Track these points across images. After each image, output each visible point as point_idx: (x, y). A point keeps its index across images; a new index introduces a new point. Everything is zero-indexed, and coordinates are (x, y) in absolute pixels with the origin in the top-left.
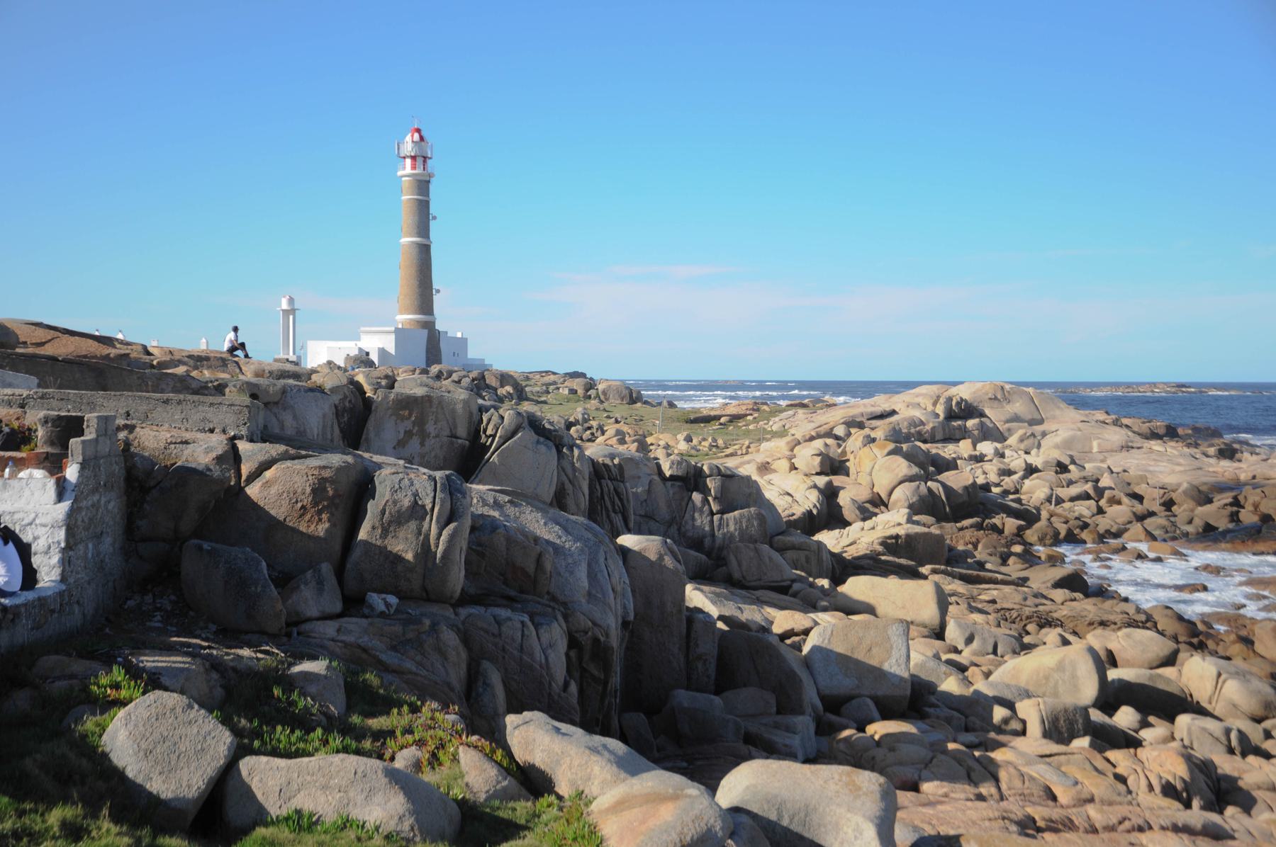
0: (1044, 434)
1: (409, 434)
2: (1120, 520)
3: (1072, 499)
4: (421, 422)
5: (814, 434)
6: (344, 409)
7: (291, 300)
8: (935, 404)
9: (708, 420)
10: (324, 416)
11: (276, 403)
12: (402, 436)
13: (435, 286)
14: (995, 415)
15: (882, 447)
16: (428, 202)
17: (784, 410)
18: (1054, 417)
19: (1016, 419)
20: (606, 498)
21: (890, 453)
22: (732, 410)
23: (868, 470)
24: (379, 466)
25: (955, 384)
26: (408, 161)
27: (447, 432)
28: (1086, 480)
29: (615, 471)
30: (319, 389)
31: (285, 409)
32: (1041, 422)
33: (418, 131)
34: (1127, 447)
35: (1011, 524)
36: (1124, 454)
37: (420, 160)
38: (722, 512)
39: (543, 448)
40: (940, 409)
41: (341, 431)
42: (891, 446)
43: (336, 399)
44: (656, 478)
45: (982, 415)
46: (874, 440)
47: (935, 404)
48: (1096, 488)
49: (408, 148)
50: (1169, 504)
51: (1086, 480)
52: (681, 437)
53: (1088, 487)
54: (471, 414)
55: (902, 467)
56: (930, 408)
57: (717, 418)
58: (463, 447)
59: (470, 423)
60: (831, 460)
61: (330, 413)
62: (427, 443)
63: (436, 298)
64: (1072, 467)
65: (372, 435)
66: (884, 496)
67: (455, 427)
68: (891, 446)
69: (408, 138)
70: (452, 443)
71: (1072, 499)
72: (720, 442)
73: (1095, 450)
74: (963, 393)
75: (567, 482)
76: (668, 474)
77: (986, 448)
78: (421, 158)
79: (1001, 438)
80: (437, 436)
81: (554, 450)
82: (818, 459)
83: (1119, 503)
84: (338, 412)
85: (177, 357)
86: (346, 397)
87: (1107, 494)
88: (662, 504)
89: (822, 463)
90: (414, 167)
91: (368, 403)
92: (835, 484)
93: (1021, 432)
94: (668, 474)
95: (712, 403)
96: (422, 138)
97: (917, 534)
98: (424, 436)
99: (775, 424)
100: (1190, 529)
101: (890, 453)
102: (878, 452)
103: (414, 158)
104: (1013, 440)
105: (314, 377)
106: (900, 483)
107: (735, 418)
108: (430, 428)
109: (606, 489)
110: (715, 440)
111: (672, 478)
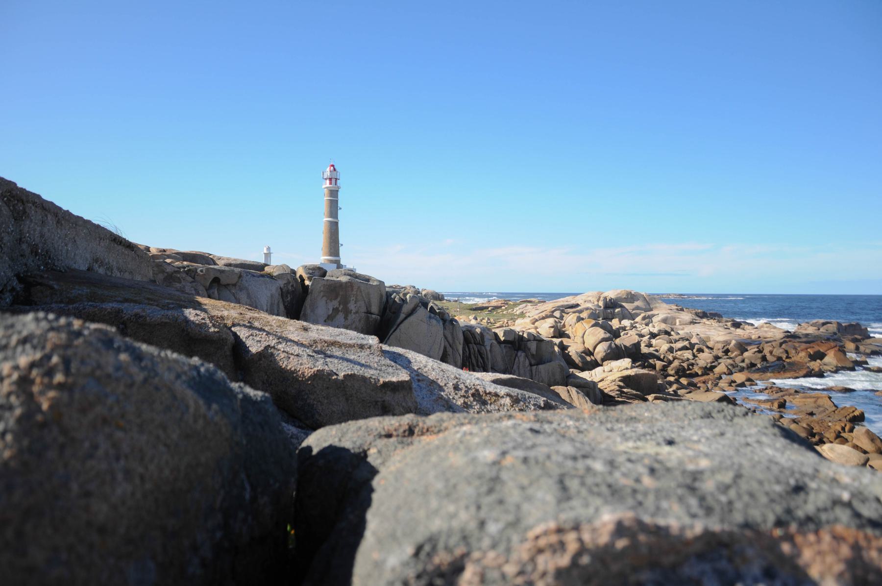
0: (653, 316)
1: (336, 310)
2: (709, 361)
3: (680, 350)
4: (345, 302)
5: (537, 317)
6: (288, 292)
7: (269, 249)
8: (598, 301)
9: (482, 309)
10: (272, 296)
11: (235, 285)
12: (330, 312)
13: (340, 242)
14: (628, 306)
15: (588, 323)
16: (337, 201)
17: (519, 304)
18: (656, 308)
19: (637, 308)
20: (473, 357)
21: (593, 326)
22: (494, 304)
23: (581, 335)
24: (632, 367)
25: (576, 294)
26: (328, 181)
27: (364, 309)
28: (683, 339)
29: (478, 338)
30: (270, 276)
31: (241, 290)
32: (651, 310)
33: (333, 166)
34: (693, 322)
35: (659, 364)
36: (692, 326)
37: (333, 181)
38: (537, 364)
39: (434, 322)
40: (601, 304)
41: (285, 307)
42: (593, 322)
43: (281, 283)
44: (494, 341)
45: (622, 306)
46: (583, 319)
47: (598, 301)
48: (690, 343)
49: (328, 174)
50: (727, 352)
51: (683, 339)
52: (471, 317)
53: (686, 343)
54: (381, 296)
55: (601, 333)
56: (596, 303)
57: (487, 308)
58: (376, 320)
59: (381, 302)
60: (559, 331)
61: (277, 295)
62: (349, 318)
63: (341, 249)
64: (672, 333)
65: (308, 311)
66: (591, 349)
67: (370, 306)
68: (593, 322)
69: (328, 169)
70: (368, 318)
71: (680, 350)
72: (492, 320)
73: (678, 323)
74: (611, 294)
75: (448, 346)
76: (502, 339)
77: (626, 323)
78: (333, 179)
79: (632, 317)
80: (357, 312)
81: (441, 323)
82: (552, 330)
83: (703, 351)
84: (283, 293)
85: (167, 253)
86: (289, 282)
87: (696, 347)
88: (499, 359)
89: (554, 332)
90: (331, 183)
91: (305, 288)
92: (565, 343)
93: (642, 315)
94: (502, 339)
95: (480, 302)
96: (335, 169)
97: (643, 374)
98: (347, 312)
99: (517, 310)
100: (743, 365)
101: (593, 326)
102: (586, 325)
103: (330, 179)
104: (638, 319)
105: (266, 269)
106: (600, 342)
107: (496, 308)
108: (352, 306)
109: (472, 351)
110: (489, 319)
111: (505, 342)
